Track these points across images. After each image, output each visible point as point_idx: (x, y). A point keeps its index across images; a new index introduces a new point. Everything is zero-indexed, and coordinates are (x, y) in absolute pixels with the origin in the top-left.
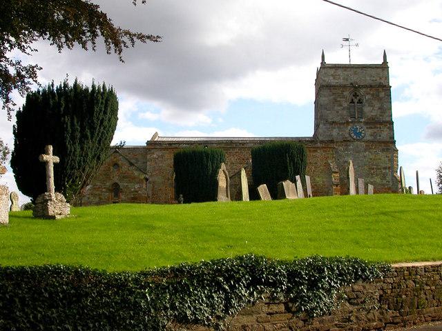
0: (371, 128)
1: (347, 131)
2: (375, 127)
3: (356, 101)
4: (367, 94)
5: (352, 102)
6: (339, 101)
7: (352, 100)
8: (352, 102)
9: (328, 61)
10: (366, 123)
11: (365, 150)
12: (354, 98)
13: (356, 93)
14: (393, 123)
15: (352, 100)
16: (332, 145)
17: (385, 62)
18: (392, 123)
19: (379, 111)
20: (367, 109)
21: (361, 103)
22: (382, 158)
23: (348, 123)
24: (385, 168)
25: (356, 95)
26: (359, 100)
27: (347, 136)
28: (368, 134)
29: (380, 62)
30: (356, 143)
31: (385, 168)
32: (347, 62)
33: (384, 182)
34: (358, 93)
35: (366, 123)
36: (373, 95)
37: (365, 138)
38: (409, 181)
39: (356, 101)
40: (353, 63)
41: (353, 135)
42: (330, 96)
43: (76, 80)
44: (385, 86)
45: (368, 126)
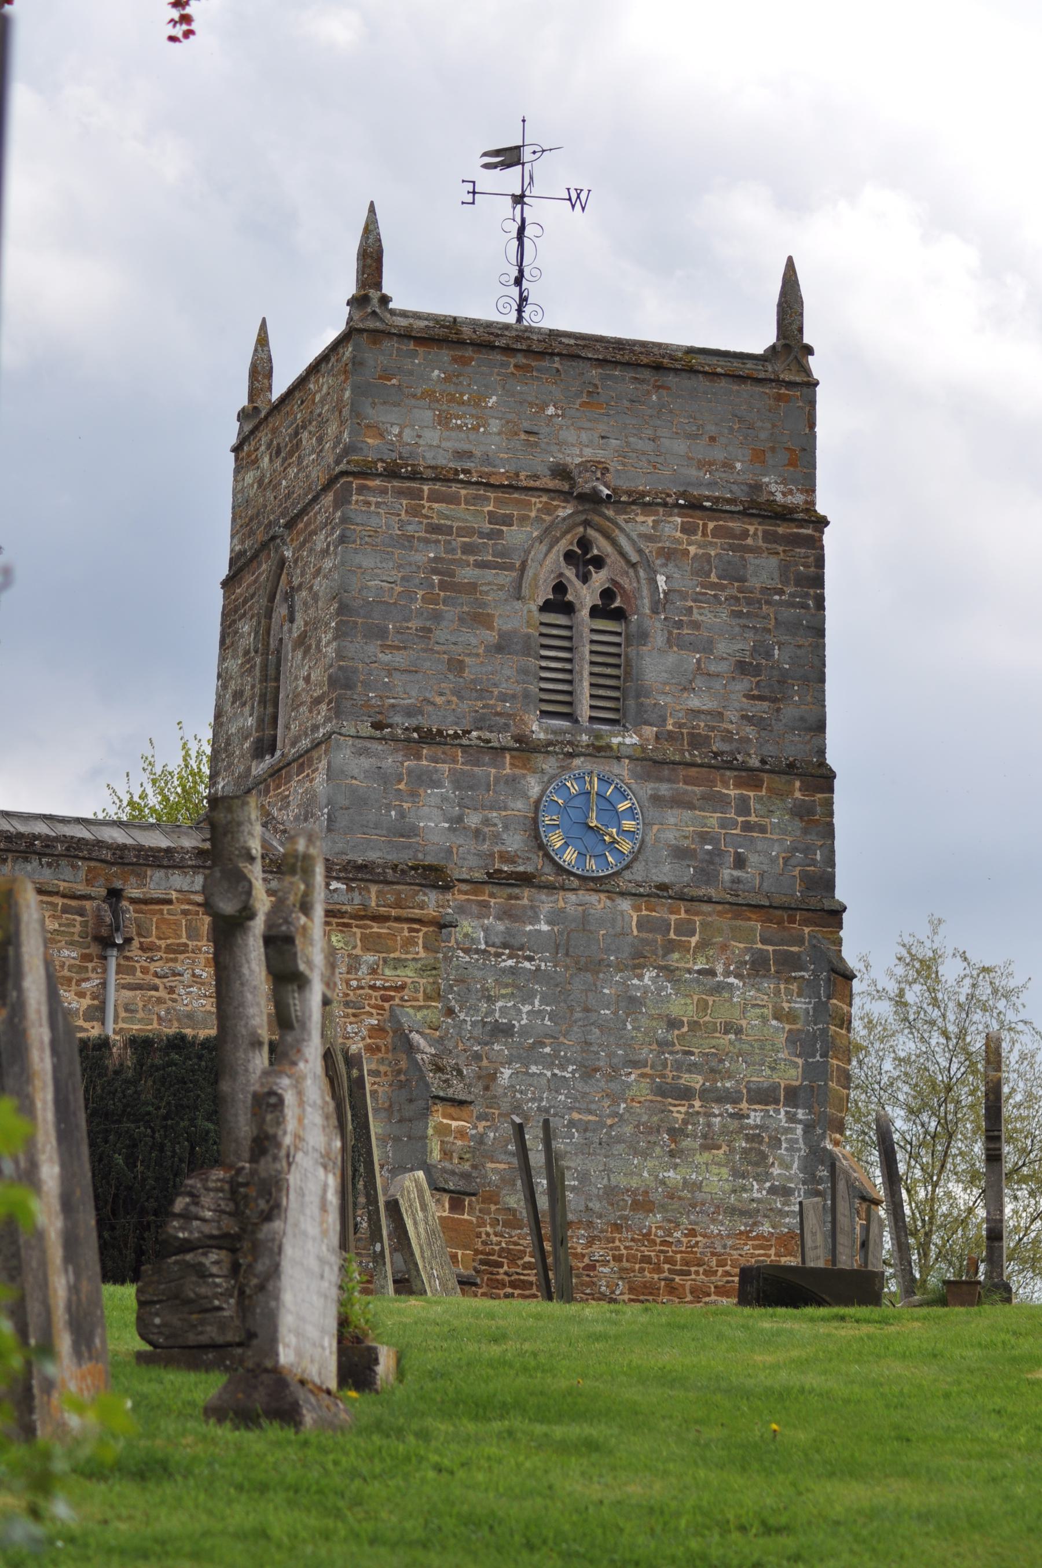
0: (679, 802)
1: (519, 807)
2: (717, 802)
3: (586, 595)
4: (669, 555)
5: (559, 603)
6: (472, 587)
7: (560, 588)
8: (559, 603)
9: (407, 292)
10: (651, 765)
11: (637, 961)
12: (570, 573)
13: (584, 543)
14: (831, 776)
15: (560, 588)
16: (431, 902)
17: (791, 344)
18: (823, 779)
19: (742, 685)
20: (657, 666)
21: (619, 615)
22: (750, 1022)
23: (526, 748)
24: (764, 1096)
25: (583, 559)
26: (607, 595)
27: (515, 842)
28: (656, 831)
29: (758, 337)
30: (570, 901)
31: (764, 1096)
32: (485, 305)
33: (758, 1191)
34: (601, 546)
35: (651, 765)
36: (702, 567)
37: (638, 872)
38: (286, 1356)
39: (586, 595)
40: (558, 313)
41: (556, 840)
42: (407, 541)
43: (371, 260)
44: (783, 514)
45: (664, 789)
